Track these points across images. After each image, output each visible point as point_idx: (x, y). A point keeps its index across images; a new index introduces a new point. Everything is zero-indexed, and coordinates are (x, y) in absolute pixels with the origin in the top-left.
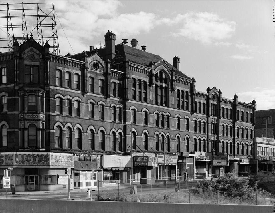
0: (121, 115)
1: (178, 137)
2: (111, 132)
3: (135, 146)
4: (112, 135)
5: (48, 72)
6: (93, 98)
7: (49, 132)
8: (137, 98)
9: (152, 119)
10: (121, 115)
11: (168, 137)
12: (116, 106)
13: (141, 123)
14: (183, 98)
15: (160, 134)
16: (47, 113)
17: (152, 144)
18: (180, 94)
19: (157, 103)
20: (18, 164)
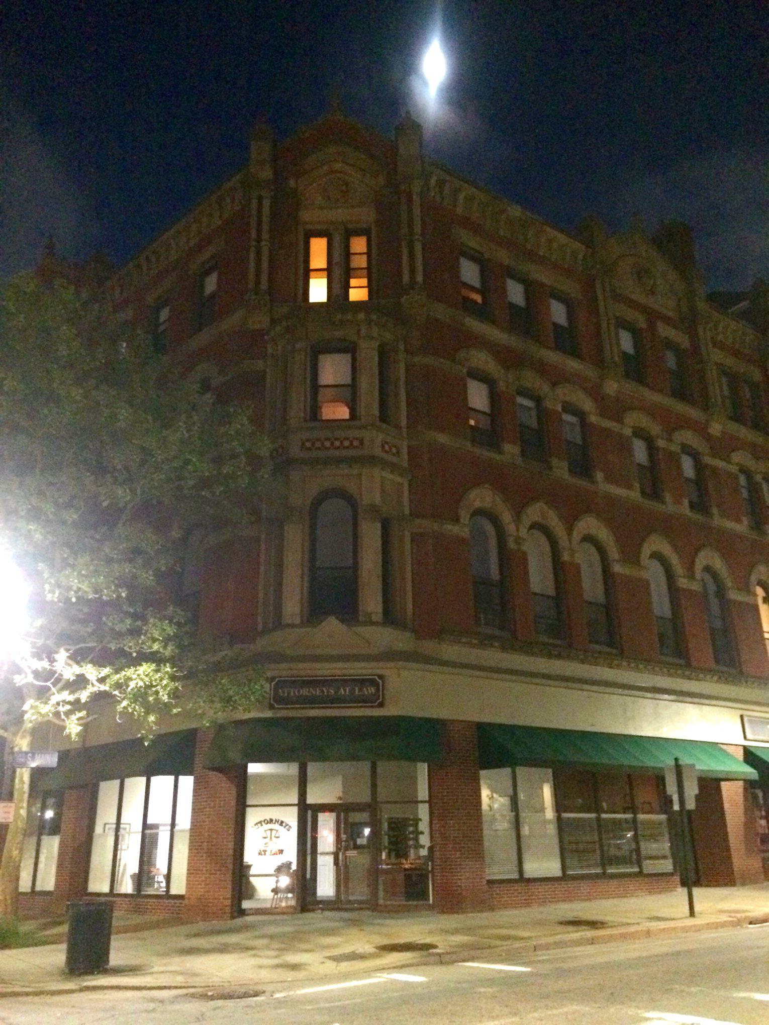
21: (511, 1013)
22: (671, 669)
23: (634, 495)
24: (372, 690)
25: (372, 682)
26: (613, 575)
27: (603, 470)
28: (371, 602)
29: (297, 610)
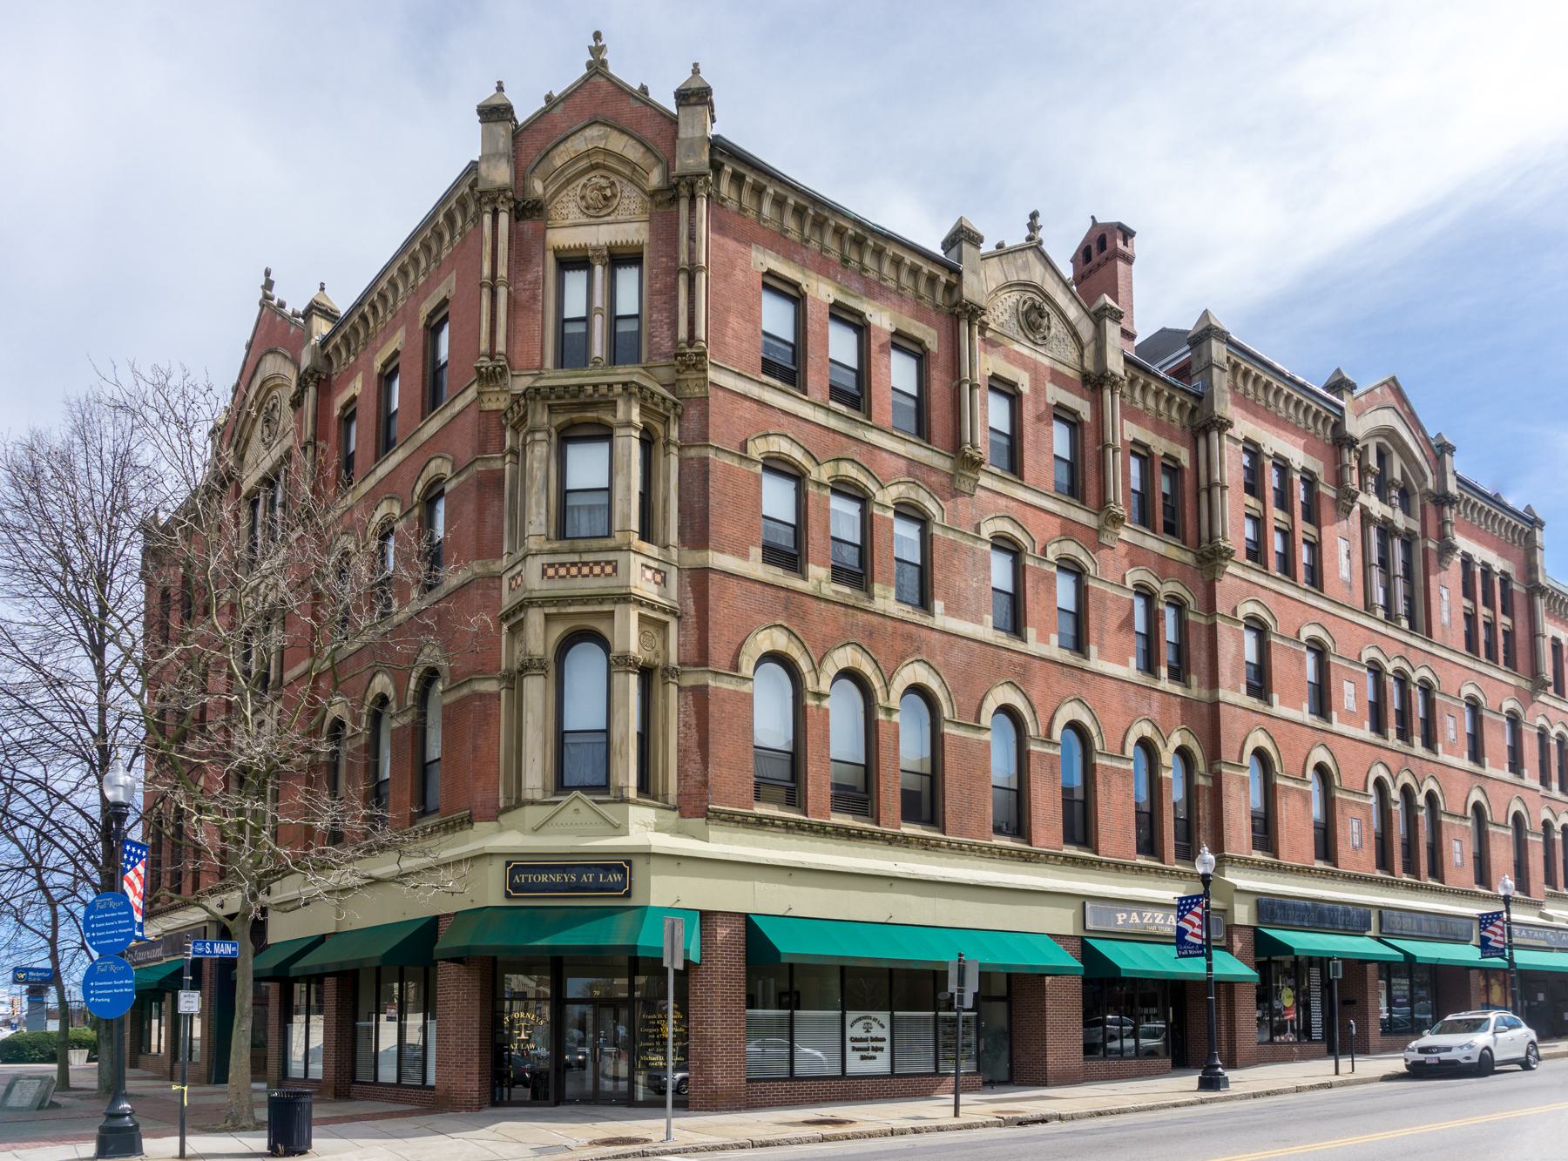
0: (1180, 652)
1: (1477, 807)
2: (1249, 749)
3: (1265, 831)
4: (1256, 762)
5: (701, 269)
6: (1265, 597)
7: (707, 686)
8: (1301, 573)
9: (1351, 694)
10: (1180, 652)
11: (1431, 797)
12: (1157, 585)
13: (1292, 707)
14: (1284, 501)
15: (1394, 780)
16: (694, 558)
17: (1355, 834)
18: (1473, 579)
19: (1369, 607)
20: (58, 878)
21: (985, 1083)
22: (846, 963)
23: (985, 630)
24: (619, 877)
25: (621, 870)
26: (1187, 622)
27: (944, 599)
28: (627, 774)
29: (539, 784)
